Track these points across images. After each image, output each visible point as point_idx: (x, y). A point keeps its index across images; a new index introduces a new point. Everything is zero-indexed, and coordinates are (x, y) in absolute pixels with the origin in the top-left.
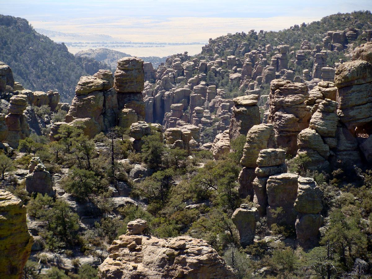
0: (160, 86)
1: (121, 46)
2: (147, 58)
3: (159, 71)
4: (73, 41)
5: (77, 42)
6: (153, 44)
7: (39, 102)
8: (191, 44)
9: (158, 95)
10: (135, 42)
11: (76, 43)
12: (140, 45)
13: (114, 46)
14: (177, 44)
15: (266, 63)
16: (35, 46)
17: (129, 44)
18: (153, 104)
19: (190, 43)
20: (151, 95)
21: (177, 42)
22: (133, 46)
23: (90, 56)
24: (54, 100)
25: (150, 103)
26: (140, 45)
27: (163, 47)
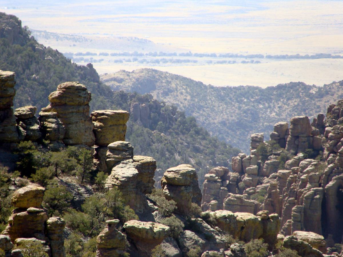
0: (336, 166)
1: (171, 61)
2: (235, 88)
3: (332, 136)
6: (237, 56)
7: (244, 233)
8: (313, 57)
9: (331, 184)
10: (199, 53)
11: (80, 54)
12: (212, 58)
13: (157, 62)
16: (43, 72)
17: (188, 57)
18: (321, 201)
19: (310, 55)
20: (318, 184)
21: (284, 54)
22: (195, 62)
23: (121, 85)
24: (271, 229)
25: (317, 199)
26: (209, 59)
27: (258, 62)
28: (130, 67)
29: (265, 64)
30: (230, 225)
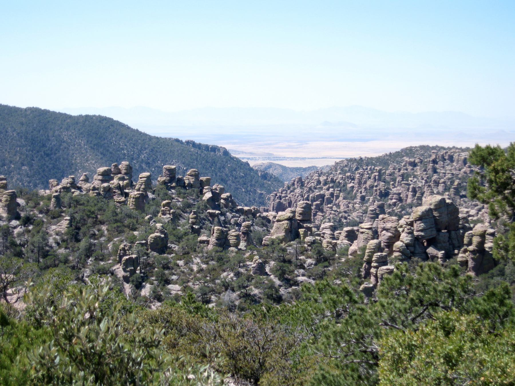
4: (251, 157)
5: (253, 157)
12: (291, 159)
14: (312, 158)
15: (369, 178)
17: (284, 159)
28: (264, 162)
29: (307, 160)
30: (358, 187)
